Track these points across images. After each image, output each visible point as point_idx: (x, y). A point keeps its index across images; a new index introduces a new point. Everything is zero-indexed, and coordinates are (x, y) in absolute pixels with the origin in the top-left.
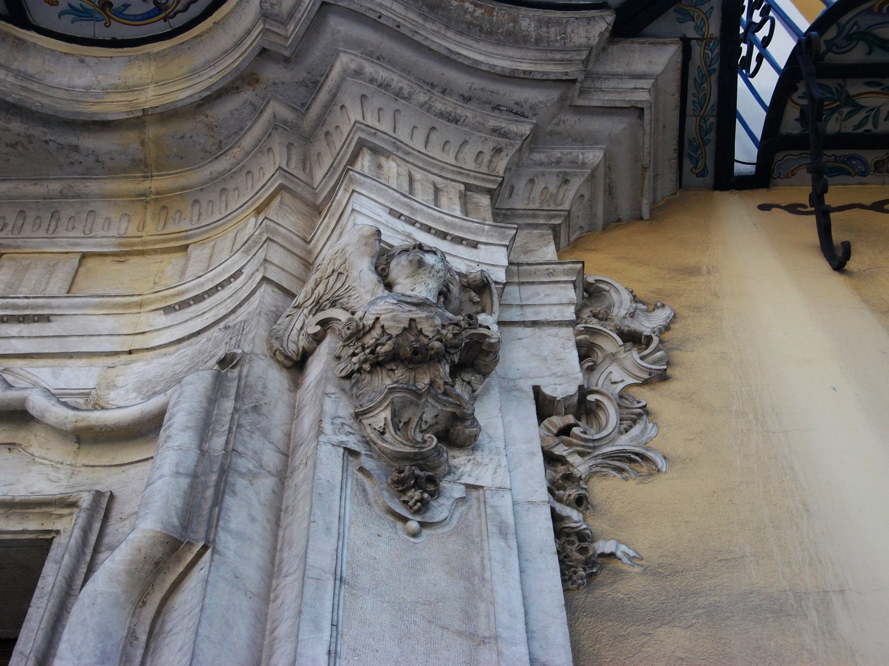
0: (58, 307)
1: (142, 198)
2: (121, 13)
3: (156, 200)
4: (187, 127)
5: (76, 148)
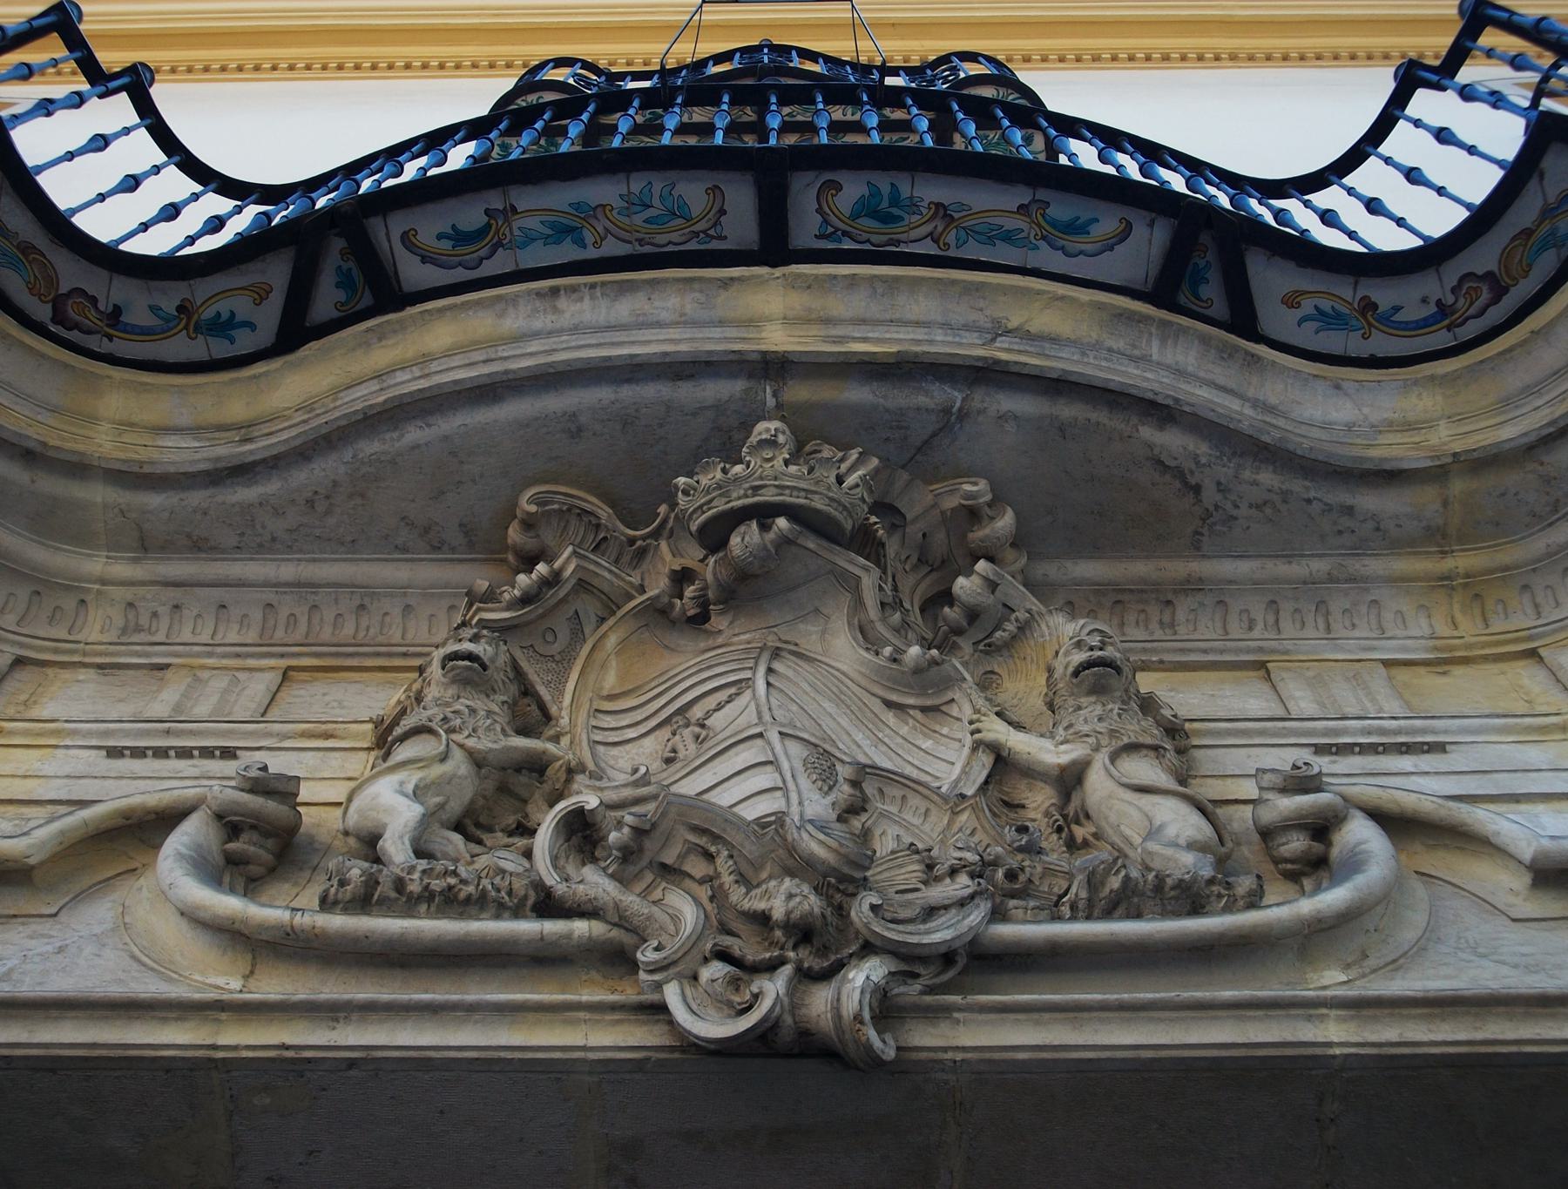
0: (1446, 732)
1: (1445, 582)
2: (1387, 319)
3: (1465, 585)
4: (1511, 479)
5: (1349, 511)
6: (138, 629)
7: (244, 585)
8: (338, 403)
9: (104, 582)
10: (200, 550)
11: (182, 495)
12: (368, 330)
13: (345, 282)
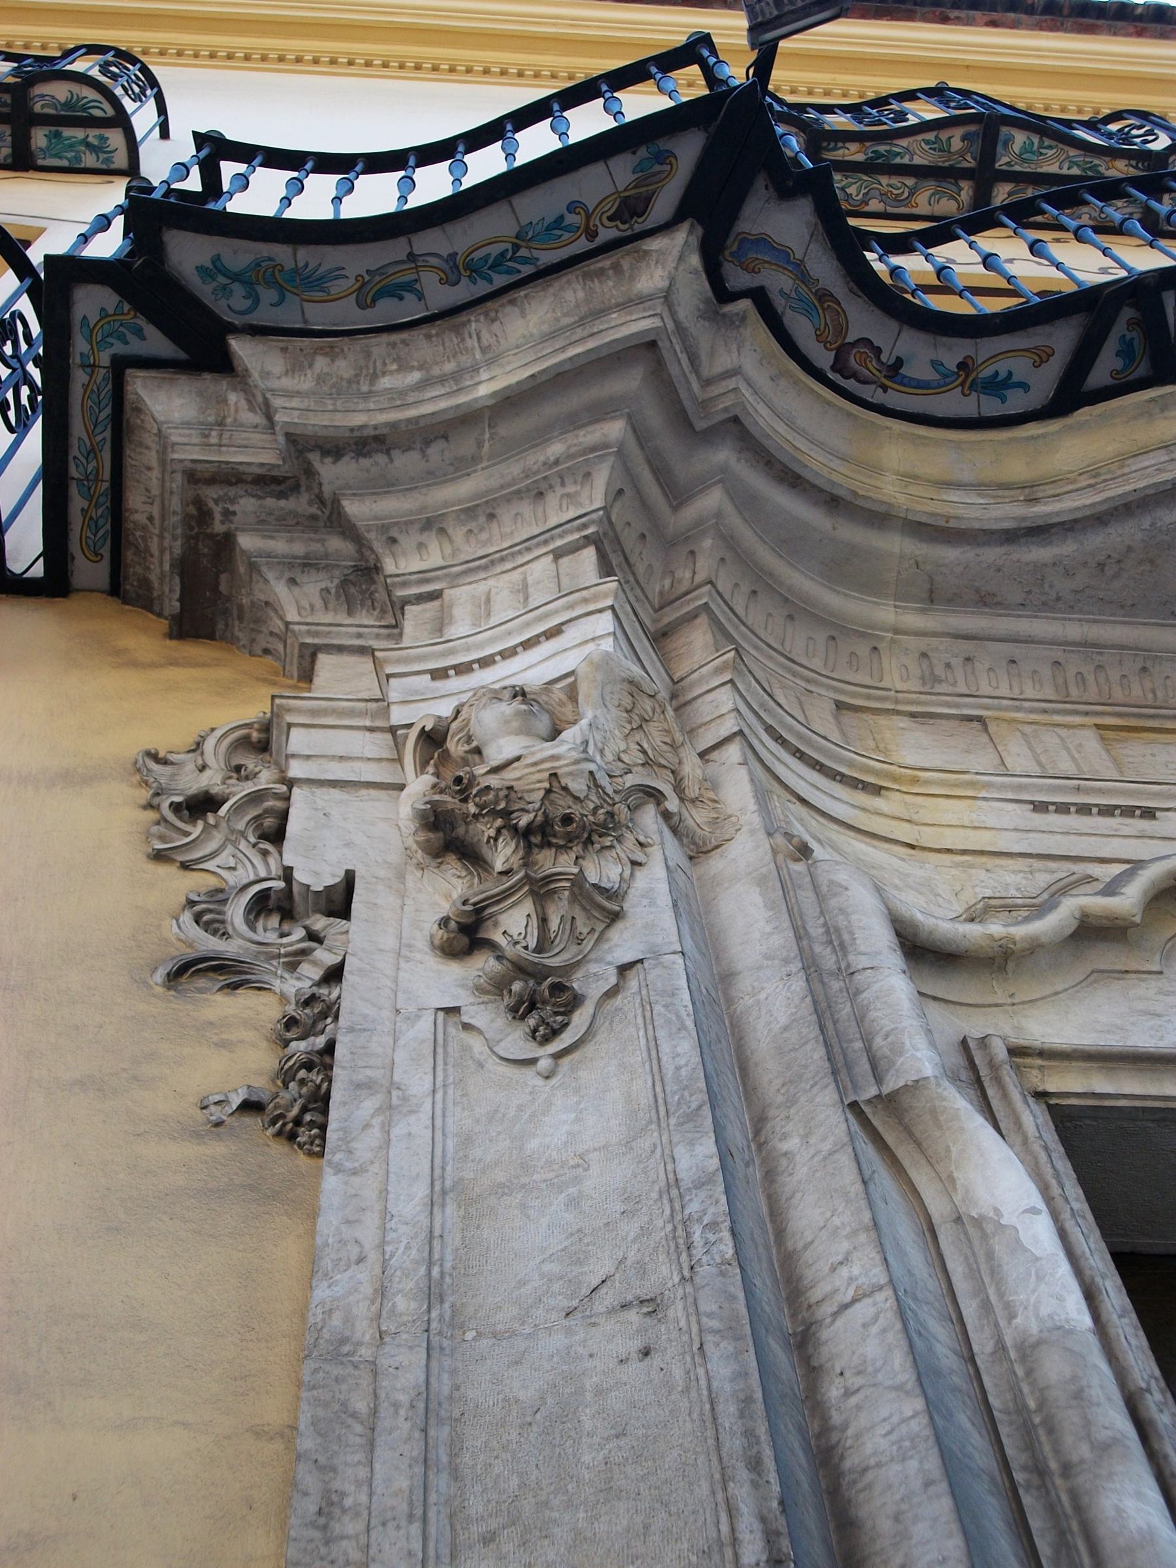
6: (937, 680)
7: (1032, 642)
8: (1126, 470)
9: (897, 631)
10: (985, 604)
11: (980, 551)
12: (1152, 400)
13: (1126, 352)
